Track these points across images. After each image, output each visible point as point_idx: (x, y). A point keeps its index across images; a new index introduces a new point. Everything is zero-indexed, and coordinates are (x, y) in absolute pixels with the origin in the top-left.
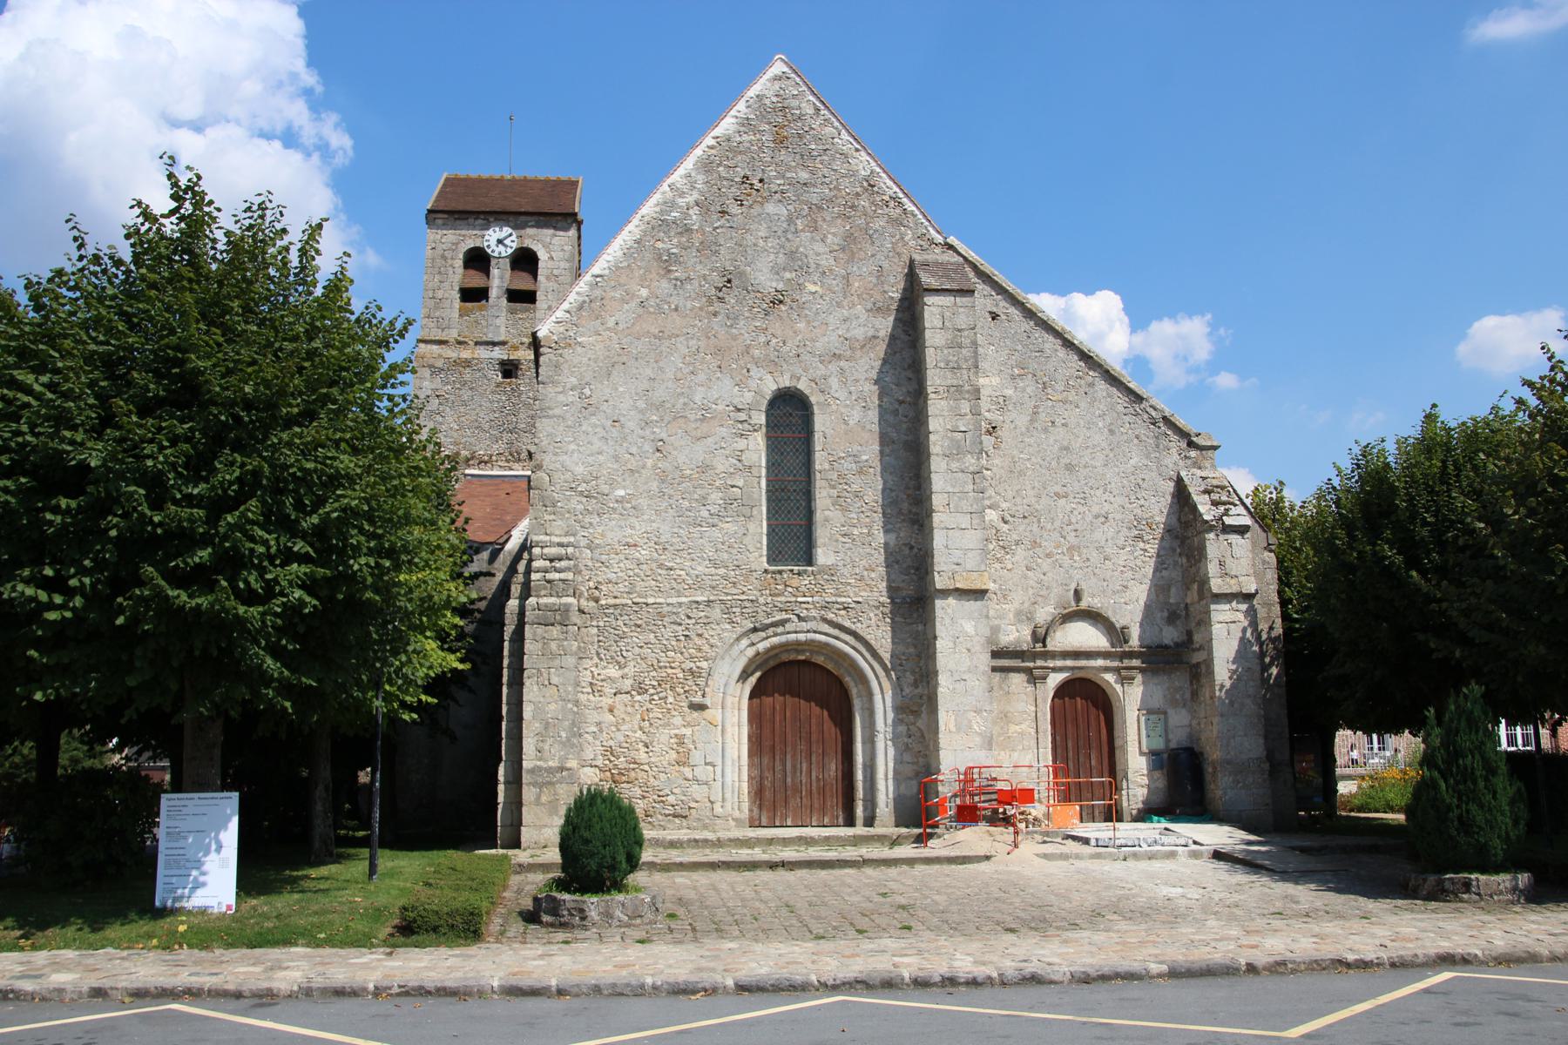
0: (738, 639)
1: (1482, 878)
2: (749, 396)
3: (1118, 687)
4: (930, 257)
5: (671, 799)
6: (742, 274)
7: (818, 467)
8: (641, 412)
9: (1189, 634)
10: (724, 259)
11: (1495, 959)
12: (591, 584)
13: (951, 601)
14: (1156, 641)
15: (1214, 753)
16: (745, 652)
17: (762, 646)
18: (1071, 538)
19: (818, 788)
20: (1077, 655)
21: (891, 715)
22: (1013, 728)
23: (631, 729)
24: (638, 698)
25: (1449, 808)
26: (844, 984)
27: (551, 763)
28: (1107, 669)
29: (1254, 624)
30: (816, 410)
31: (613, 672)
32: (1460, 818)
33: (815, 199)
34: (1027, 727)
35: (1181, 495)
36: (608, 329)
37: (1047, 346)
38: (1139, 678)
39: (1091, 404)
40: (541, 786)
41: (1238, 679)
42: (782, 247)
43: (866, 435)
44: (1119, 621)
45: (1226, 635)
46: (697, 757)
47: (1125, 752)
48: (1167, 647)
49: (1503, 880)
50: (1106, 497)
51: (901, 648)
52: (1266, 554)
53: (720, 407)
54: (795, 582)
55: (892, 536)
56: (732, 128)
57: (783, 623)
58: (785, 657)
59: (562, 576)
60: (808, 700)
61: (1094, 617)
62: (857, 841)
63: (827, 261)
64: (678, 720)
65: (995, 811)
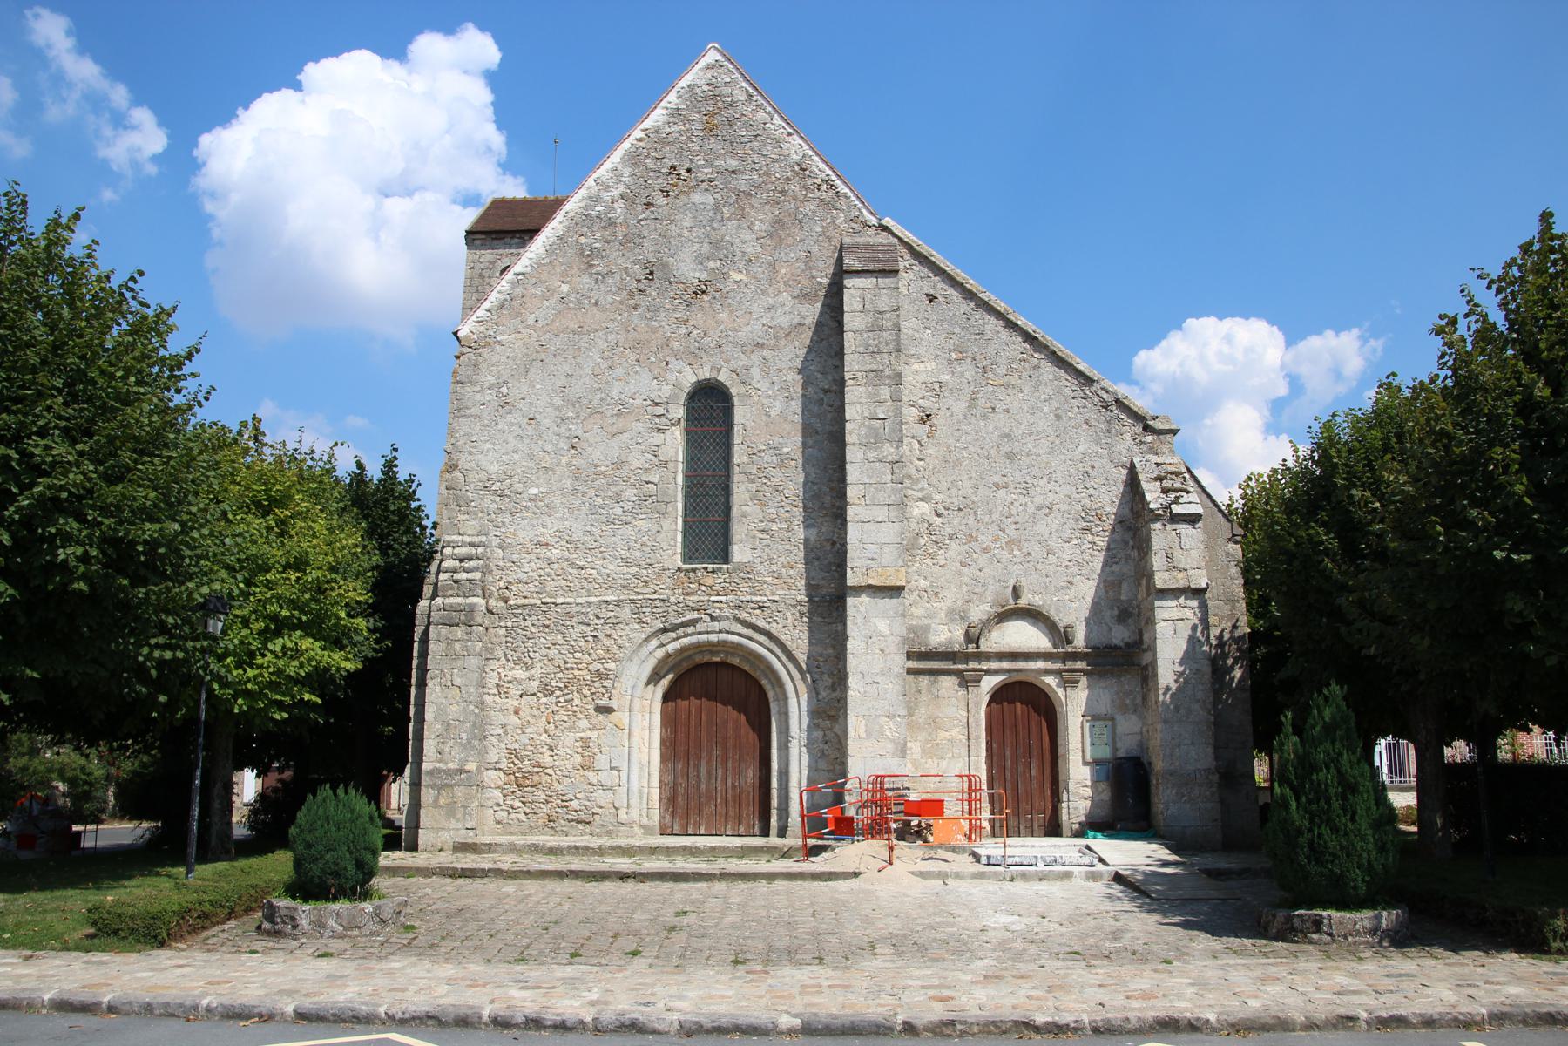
0: (647, 640)
1: (1335, 914)
2: (667, 390)
3: (1060, 691)
4: (861, 240)
5: (575, 804)
6: (665, 266)
7: (736, 460)
8: (558, 409)
9: (1141, 633)
10: (648, 251)
11: (1233, 1026)
12: (502, 584)
13: (864, 598)
14: (1104, 641)
15: (1159, 765)
16: (654, 653)
17: (671, 648)
18: (1011, 530)
19: (734, 796)
20: (1014, 656)
21: (806, 720)
22: (942, 735)
23: (536, 732)
24: (544, 700)
25: (1299, 832)
26: (414, 1018)
27: (450, 766)
28: (1047, 672)
29: (1204, 621)
30: (736, 401)
31: (520, 673)
32: (1311, 843)
33: (743, 186)
34: (958, 734)
35: (1133, 484)
36: (528, 327)
37: (988, 327)
38: (1084, 681)
39: (1036, 388)
40: (439, 788)
41: (1185, 683)
42: (708, 236)
43: (788, 427)
44: (1062, 620)
45: (1172, 637)
46: (602, 761)
47: (1067, 761)
48: (1116, 648)
49: (1364, 918)
50: (1050, 486)
51: (819, 649)
52: (1231, 545)
53: (638, 402)
54: (709, 580)
55: (813, 532)
56: (662, 119)
57: (693, 623)
58: (699, 659)
59: (470, 576)
60: (724, 704)
61: (1033, 615)
62: (770, 851)
63: (753, 249)
64: (583, 723)
65: (907, 823)
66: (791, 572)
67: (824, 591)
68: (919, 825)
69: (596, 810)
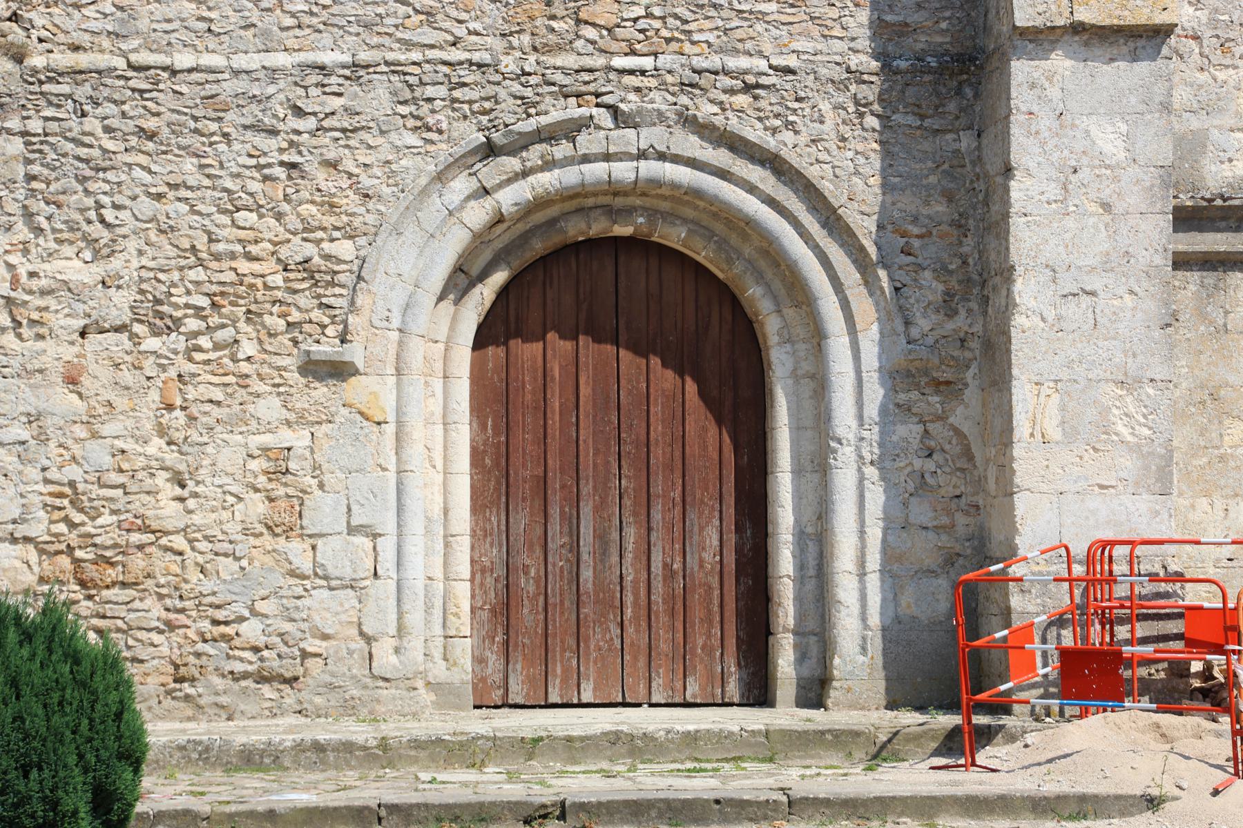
0: (441, 177)
5: (251, 630)
13: (1060, 63)
16: (461, 214)
17: (510, 198)
19: (670, 598)
21: (875, 393)
24: (152, 343)
31: (75, 269)
46: (324, 511)
51: (908, 203)
57: (570, 130)
58: (576, 230)
60: (640, 350)
64: (269, 408)
65: (1179, 670)
67: (921, 42)
68: (1207, 674)
69: (313, 645)
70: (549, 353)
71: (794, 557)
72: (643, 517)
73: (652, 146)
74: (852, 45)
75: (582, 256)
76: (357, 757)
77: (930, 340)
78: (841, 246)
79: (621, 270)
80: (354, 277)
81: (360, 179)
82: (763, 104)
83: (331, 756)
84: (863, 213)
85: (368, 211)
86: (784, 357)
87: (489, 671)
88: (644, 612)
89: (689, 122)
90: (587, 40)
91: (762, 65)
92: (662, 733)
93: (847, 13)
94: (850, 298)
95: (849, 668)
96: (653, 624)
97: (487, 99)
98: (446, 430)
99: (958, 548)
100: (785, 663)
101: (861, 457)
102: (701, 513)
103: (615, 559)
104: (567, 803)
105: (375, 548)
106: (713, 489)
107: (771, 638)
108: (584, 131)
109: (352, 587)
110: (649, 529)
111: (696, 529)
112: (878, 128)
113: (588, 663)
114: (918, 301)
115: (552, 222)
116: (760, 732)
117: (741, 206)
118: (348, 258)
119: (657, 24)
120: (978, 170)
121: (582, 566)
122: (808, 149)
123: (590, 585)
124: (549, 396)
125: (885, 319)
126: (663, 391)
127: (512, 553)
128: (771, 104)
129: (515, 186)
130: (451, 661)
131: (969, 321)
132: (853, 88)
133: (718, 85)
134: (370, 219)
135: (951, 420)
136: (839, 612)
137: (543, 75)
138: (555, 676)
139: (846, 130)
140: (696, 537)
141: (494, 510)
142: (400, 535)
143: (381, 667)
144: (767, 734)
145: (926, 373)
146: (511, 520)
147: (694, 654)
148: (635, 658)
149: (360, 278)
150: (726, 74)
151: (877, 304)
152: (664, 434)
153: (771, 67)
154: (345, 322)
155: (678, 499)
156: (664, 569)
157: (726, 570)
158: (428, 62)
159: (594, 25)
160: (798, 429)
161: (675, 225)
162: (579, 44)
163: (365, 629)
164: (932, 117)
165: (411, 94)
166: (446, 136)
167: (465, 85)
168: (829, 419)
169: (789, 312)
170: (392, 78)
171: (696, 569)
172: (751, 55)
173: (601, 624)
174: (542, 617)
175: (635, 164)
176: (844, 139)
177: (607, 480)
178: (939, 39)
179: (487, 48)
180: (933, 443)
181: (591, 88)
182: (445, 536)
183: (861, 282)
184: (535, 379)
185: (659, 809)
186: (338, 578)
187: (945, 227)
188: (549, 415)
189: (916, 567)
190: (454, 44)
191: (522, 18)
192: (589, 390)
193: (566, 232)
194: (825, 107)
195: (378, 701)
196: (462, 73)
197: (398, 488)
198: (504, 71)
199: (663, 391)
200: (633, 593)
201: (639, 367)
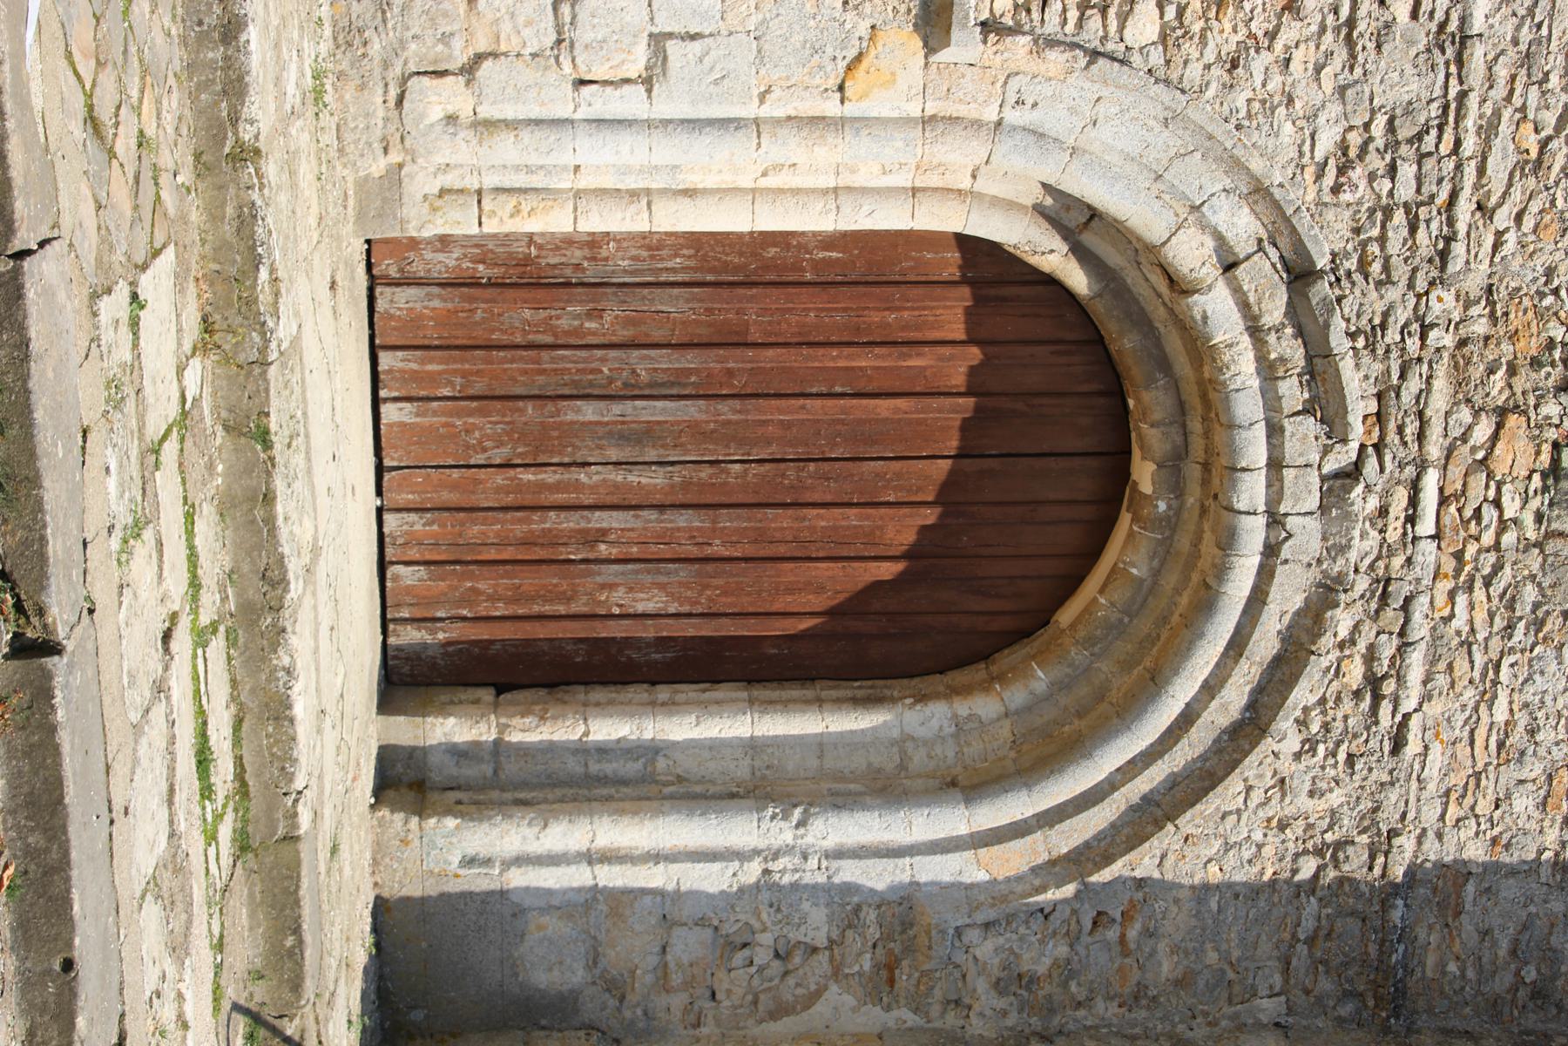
0: (1259, 193)
21: (878, 877)
51: (1176, 923)
57: (1325, 405)
58: (1149, 404)
66: (1523, 803)
67: (1429, 936)
70: (946, 351)
71: (619, 741)
72: (681, 498)
73: (1290, 536)
74: (1431, 834)
75: (1102, 401)
76: (216, 104)
77: (960, 957)
78: (1113, 825)
79: (1077, 461)
80: (1096, 44)
81: (1264, 53)
82: (1347, 705)
83: (216, 54)
84: (1163, 856)
85: (1208, 67)
86: (935, 724)
87: (428, 255)
88: (528, 499)
89: (1327, 594)
90: (1470, 428)
91: (1408, 705)
92: (286, 661)
93: (1483, 827)
94: (1028, 839)
95: (440, 842)
96: (509, 515)
97: (1386, 268)
98: (825, 192)
99: (632, 998)
100: (449, 729)
101: (776, 856)
102: (687, 586)
103: (614, 454)
104: (51, 662)
105: (627, 81)
106: (726, 604)
107: (487, 695)
108: (1320, 429)
109: (559, 42)
110: (661, 507)
111: (663, 579)
112: (1297, 878)
113: (444, 414)
114: (1022, 939)
115: (1164, 364)
116: (295, 826)
117: (1184, 674)
118: (1127, 34)
119: (1488, 538)
120: (1224, 1023)
121: (602, 404)
122: (1269, 774)
123: (570, 417)
124: (877, 350)
125: (996, 891)
126: (881, 528)
127: (621, 292)
128: (1346, 718)
129: (1236, 316)
130: (439, 203)
131: (988, 1012)
132: (1364, 839)
133: (1384, 637)
134: (1194, 72)
135: (834, 988)
136: (530, 824)
137: (1419, 360)
138: (423, 362)
139: (1298, 828)
140: (649, 579)
141: (692, 263)
142: (649, 124)
143: (421, 91)
144: (291, 839)
145: (909, 949)
146: (676, 291)
147: (463, 577)
148: (454, 487)
149: (1094, 55)
150: (1399, 650)
151: (1019, 879)
152: (812, 529)
153: (1407, 717)
154: (1016, 30)
155: (709, 551)
156: (598, 530)
157: (597, 624)
158: (1459, 167)
159: (1495, 438)
160: (821, 745)
161: (1152, 558)
162: (1465, 415)
163: (487, 65)
164: (1311, 955)
165: (1402, 138)
166: (1327, 198)
167: (1413, 229)
168: (837, 807)
169: (1005, 731)
170: (1435, 105)
171: (599, 579)
172: (1425, 683)
173: (508, 433)
174: (519, 339)
175: (1262, 508)
176: (1282, 826)
177: (741, 442)
178: (1431, 960)
179: (1472, 267)
180: (797, 960)
181: (1392, 437)
182: (648, 192)
183: (1055, 854)
184: (905, 328)
185: (47, 850)
186: (574, 17)
187: (1135, 975)
188: (847, 351)
189: (602, 937)
190: (1480, 207)
191: (1516, 321)
192: (885, 414)
193: (1147, 388)
194: (1336, 798)
195: (362, 87)
196: (1434, 225)
197: (729, 121)
198: (1433, 296)
199: (881, 528)
200: (559, 482)
201: (919, 489)
